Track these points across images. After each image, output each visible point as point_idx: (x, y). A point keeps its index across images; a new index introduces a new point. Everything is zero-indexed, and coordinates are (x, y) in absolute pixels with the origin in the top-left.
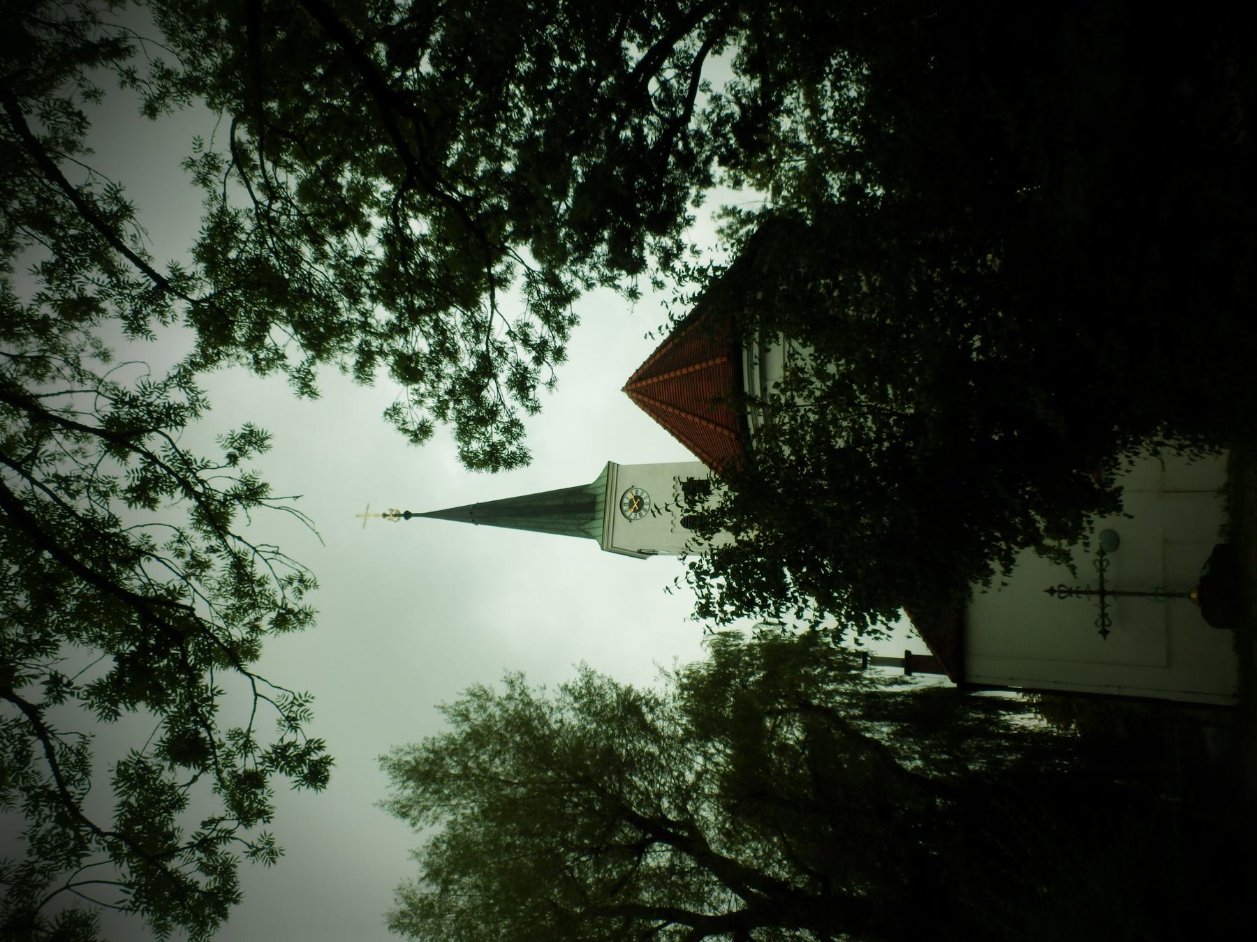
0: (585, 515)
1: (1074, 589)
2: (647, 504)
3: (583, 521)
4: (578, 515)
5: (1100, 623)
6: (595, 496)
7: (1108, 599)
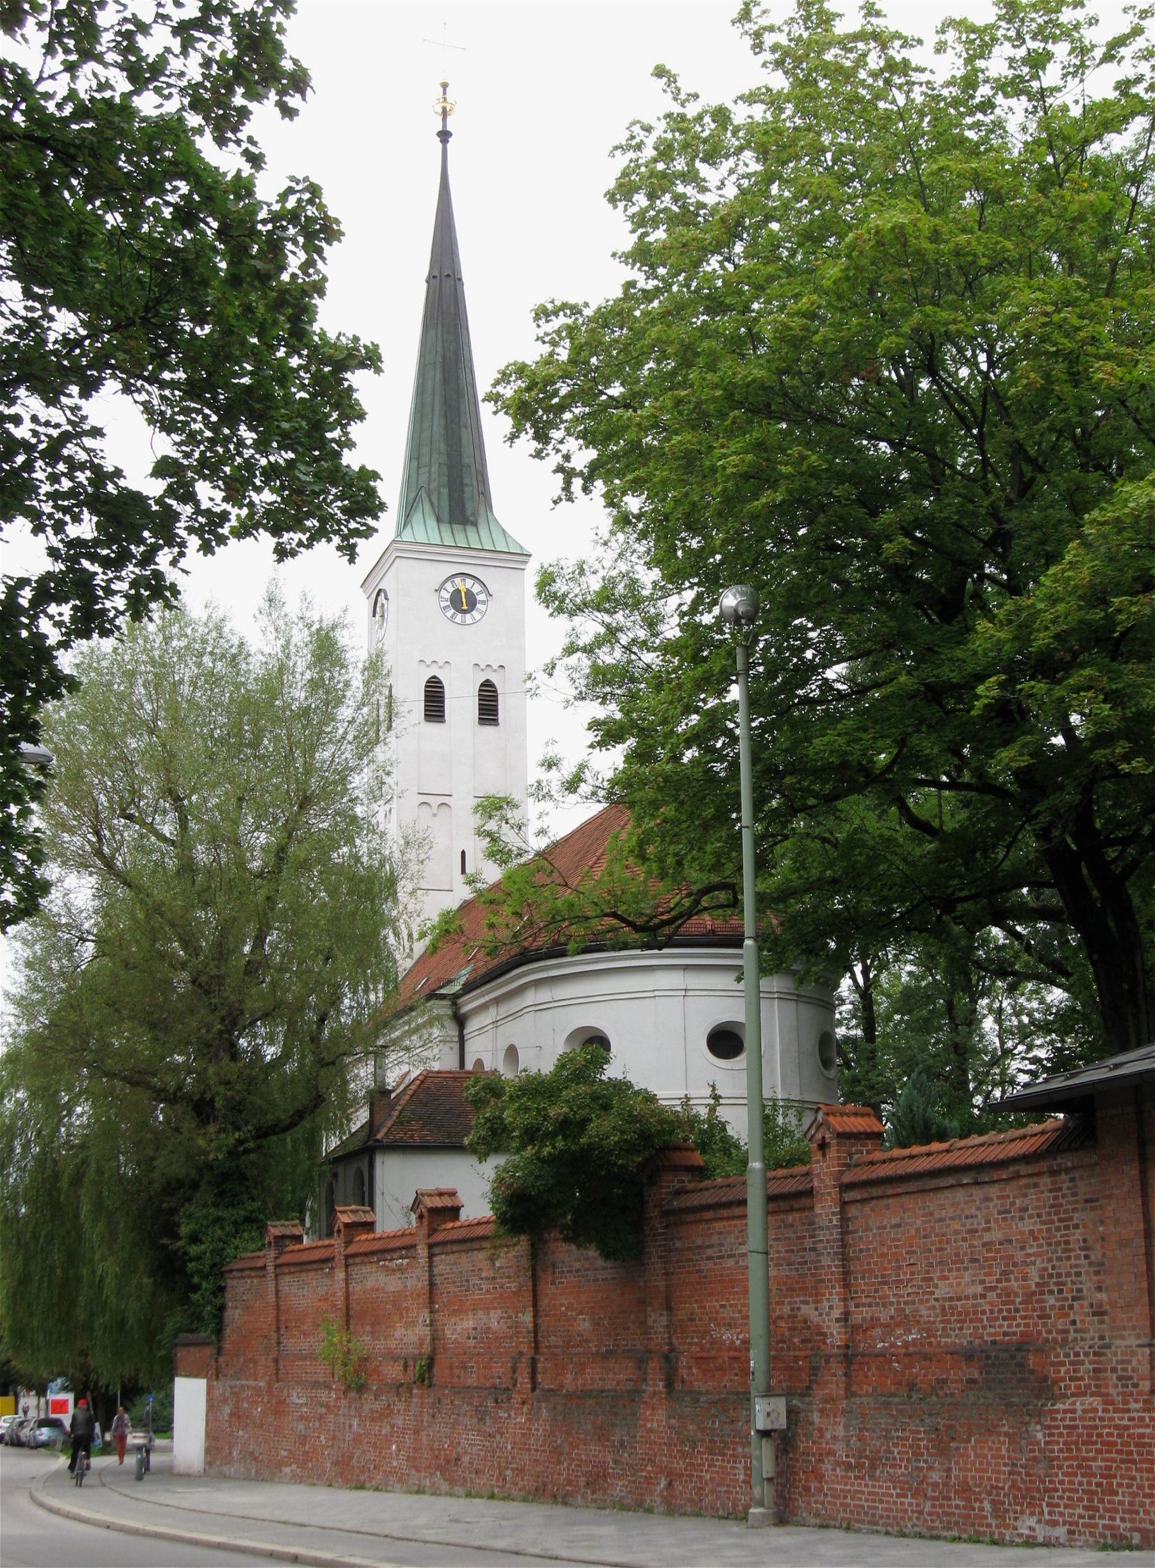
0: (445, 504)
4: (445, 491)
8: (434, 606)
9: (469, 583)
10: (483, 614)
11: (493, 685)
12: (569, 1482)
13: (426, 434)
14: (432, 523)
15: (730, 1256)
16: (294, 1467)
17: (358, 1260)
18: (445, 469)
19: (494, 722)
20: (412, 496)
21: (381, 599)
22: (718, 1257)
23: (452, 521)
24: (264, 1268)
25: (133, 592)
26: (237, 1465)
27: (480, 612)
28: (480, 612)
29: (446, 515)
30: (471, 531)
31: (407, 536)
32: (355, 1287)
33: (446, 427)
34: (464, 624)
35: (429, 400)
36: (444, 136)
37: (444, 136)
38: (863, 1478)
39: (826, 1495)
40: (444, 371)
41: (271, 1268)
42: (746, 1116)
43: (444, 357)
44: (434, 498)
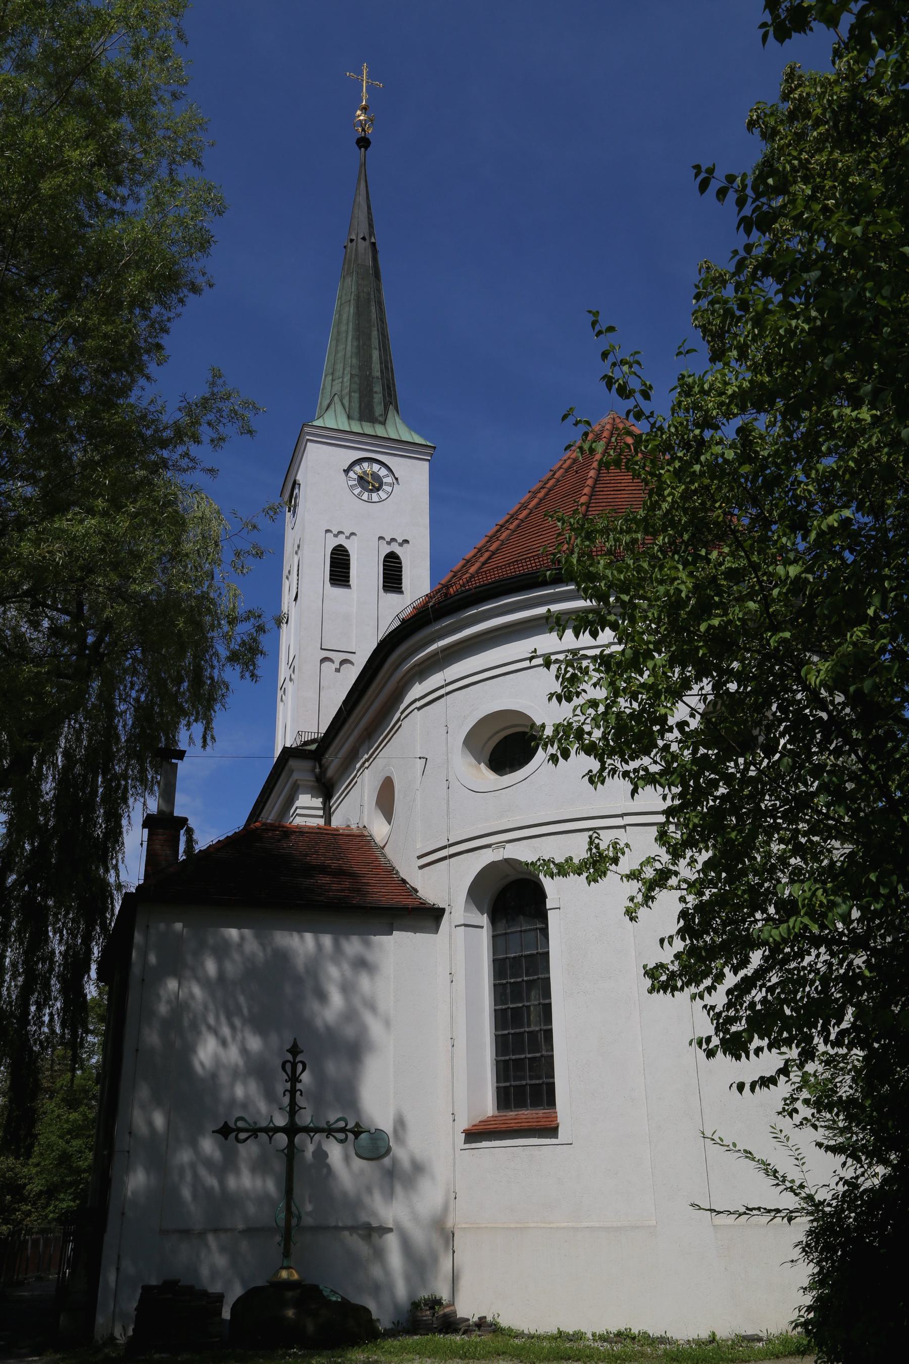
0: (356, 405)
1: (299, 1086)
2: (370, 497)
3: (347, 404)
4: (356, 396)
5: (240, 1124)
6: (384, 423)
7: (282, 1139)
9: (376, 467)
11: (397, 557)
13: (340, 354)
18: (356, 379)
25: (765, 915)
27: (387, 492)
29: (356, 414)
35: (343, 328)
40: (357, 307)
42: (398, 936)
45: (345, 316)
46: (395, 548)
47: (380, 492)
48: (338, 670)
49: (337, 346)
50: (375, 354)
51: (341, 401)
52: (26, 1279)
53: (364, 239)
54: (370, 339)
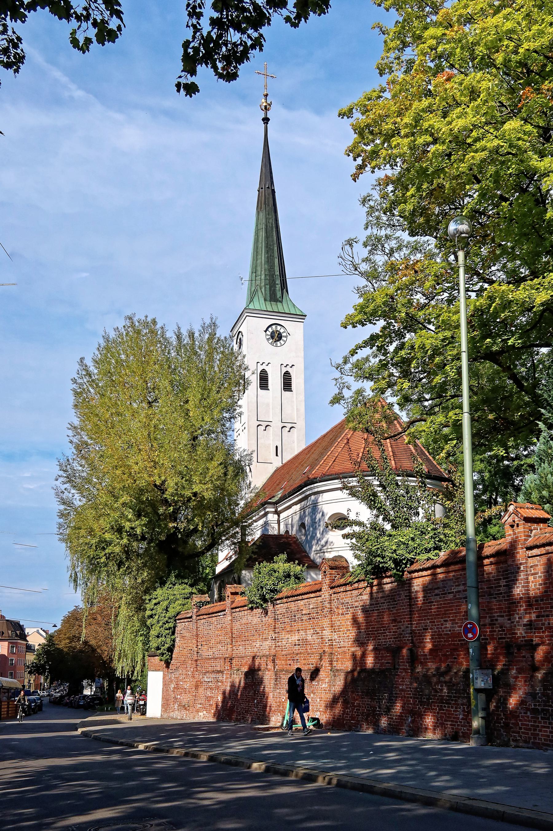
0: (268, 293)
4: (268, 287)
8: (263, 337)
9: (279, 328)
10: (285, 342)
11: (289, 374)
12: (353, 718)
14: (262, 300)
15: (449, 593)
16: (205, 712)
17: (237, 610)
18: (268, 277)
19: (290, 390)
20: (253, 289)
21: (240, 336)
22: (442, 594)
23: (270, 301)
24: (191, 617)
26: (177, 712)
27: (284, 341)
28: (284, 341)
29: (268, 298)
30: (279, 304)
31: (251, 306)
32: (237, 626)
33: (268, 257)
34: (276, 346)
36: (266, 120)
37: (266, 120)
38: (548, 719)
39: (521, 728)
40: (266, 232)
41: (194, 617)
43: (266, 226)
44: (263, 290)
45: (260, 238)
46: (288, 369)
47: (281, 341)
48: (289, 431)
49: (257, 256)
50: (276, 261)
51: (261, 289)
52: (389, 623)
53: (268, 188)
54: (273, 253)
